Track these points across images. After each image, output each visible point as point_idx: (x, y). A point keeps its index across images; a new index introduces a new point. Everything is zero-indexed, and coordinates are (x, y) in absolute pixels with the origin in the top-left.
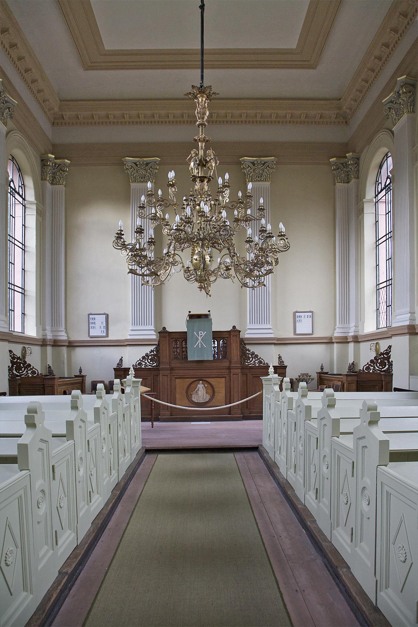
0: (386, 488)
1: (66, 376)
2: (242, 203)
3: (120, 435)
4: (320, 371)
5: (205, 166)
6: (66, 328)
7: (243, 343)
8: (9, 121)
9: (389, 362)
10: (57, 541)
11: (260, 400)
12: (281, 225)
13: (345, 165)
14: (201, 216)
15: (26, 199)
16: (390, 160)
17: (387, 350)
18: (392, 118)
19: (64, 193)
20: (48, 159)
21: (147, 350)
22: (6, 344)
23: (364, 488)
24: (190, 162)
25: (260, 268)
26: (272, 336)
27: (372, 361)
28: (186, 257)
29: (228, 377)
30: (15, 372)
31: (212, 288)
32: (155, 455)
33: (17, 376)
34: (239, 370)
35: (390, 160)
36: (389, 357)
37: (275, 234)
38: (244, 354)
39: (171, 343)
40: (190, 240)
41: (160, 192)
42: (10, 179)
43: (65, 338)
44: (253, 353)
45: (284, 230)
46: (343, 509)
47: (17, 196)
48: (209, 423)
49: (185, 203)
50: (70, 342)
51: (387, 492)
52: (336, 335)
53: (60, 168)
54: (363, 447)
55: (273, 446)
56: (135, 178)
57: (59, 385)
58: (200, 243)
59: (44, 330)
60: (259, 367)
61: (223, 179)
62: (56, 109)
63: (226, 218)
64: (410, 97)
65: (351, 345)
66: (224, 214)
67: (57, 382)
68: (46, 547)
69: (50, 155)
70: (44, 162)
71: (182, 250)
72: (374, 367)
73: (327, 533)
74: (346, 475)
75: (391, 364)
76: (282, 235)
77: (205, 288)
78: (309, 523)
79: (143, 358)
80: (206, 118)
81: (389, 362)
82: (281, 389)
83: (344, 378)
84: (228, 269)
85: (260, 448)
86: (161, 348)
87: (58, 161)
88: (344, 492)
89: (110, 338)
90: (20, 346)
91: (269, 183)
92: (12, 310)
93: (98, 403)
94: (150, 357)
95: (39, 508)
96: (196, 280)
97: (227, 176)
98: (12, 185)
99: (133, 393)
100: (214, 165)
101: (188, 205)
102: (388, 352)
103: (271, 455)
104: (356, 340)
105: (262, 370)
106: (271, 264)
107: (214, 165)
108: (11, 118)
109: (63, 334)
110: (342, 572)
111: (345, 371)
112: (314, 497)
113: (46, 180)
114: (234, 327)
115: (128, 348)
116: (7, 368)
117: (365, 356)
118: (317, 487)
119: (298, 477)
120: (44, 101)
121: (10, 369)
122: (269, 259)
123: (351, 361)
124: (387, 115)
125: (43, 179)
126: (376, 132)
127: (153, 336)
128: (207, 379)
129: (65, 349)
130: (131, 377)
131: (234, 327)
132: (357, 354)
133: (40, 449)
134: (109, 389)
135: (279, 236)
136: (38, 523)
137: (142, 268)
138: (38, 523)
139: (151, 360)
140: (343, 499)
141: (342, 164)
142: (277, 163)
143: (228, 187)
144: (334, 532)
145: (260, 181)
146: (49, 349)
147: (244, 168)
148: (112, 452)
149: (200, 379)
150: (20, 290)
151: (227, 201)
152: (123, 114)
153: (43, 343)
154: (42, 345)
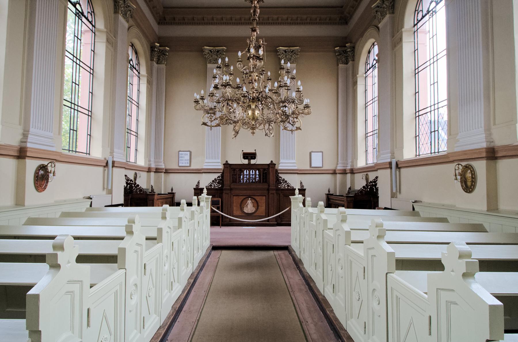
0: (395, 293)
1: (163, 193)
3: (195, 236)
4: (327, 193)
6: (164, 161)
8: (130, 19)
9: (376, 188)
10: (144, 325)
11: (289, 212)
13: (345, 52)
15: (96, 26)
16: (376, 48)
20: (155, 47)
21: (216, 176)
22: (123, 170)
23: (374, 290)
26: (296, 168)
34: (275, 191)
35: (376, 48)
36: (376, 185)
38: (278, 180)
39: (231, 171)
42: (130, 58)
43: (163, 167)
44: (284, 180)
46: (356, 305)
47: (134, 70)
50: (166, 170)
51: (397, 297)
52: (339, 168)
54: (372, 256)
55: (298, 246)
57: (158, 199)
59: (150, 161)
60: (288, 189)
62: (161, 13)
65: (349, 176)
67: (156, 197)
68: (135, 331)
69: (156, 44)
70: (152, 48)
73: (322, 291)
74: (358, 276)
78: (328, 312)
79: (213, 181)
81: (376, 188)
82: (304, 205)
86: (225, 174)
87: (161, 48)
88: (356, 290)
90: (133, 172)
91: (295, 65)
98: (131, 63)
103: (297, 253)
104: (352, 172)
105: (290, 192)
108: (132, 17)
109: (162, 164)
110: (342, 333)
112: (363, 333)
113: (153, 60)
114: (272, 161)
115: (204, 174)
117: (360, 183)
118: (333, 283)
119: (318, 273)
120: (153, 8)
123: (348, 186)
124: (375, 16)
125: (152, 60)
126: (366, 30)
127: (221, 167)
128: (253, 197)
129: (163, 174)
130: (204, 195)
132: (353, 182)
133: (136, 251)
136: (130, 311)
139: (218, 183)
140: (355, 296)
144: (349, 322)
146: (152, 174)
148: (189, 250)
150: (135, 134)
152: (203, 18)
153: (149, 170)
154: (147, 172)
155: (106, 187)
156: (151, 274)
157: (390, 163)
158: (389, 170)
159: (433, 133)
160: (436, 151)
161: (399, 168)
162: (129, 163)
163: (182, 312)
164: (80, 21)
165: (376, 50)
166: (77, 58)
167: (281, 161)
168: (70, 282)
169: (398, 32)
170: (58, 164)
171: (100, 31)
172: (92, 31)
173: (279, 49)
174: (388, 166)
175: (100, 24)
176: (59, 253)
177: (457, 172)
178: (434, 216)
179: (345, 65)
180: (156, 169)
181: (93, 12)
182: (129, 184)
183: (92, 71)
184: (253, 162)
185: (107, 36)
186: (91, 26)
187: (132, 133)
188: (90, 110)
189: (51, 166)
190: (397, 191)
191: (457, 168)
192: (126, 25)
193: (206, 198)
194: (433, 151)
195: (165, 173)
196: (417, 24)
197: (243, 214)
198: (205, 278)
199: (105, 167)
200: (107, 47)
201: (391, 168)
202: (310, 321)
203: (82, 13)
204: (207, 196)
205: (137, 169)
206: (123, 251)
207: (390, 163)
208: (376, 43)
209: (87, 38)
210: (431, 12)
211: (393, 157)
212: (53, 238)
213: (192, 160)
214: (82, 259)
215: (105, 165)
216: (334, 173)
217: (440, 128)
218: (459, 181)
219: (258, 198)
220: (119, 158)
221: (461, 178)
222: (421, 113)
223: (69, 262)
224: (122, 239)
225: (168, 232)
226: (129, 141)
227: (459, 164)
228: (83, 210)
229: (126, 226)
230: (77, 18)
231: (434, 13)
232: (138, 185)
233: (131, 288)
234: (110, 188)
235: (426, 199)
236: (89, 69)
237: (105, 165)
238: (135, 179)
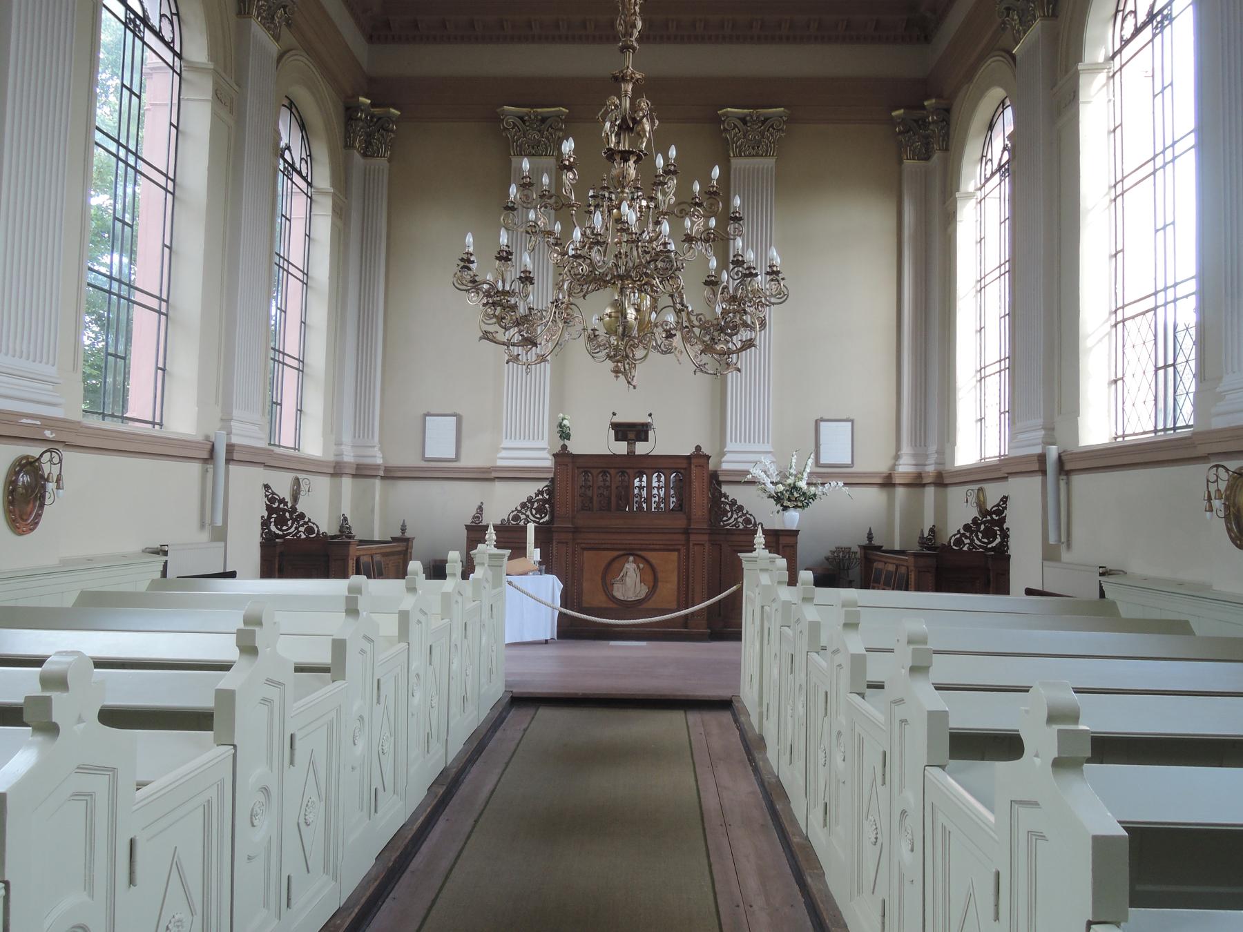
0: (941, 819)
1: (376, 538)
2: (700, 205)
3: (454, 666)
4: (866, 542)
5: (631, 130)
6: (381, 442)
7: (715, 480)
8: (285, 31)
9: (1002, 529)
10: (289, 899)
11: (736, 599)
12: (774, 253)
13: (922, 123)
14: (622, 230)
15: (184, 55)
16: (1009, 113)
17: (998, 505)
18: (1013, 28)
19: (386, 172)
24: (604, 122)
25: (731, 336)
27: (966, 527)
28: (596, 310)
29: (683, 551)
30: (273, 528)
31: (640, 372)
32: (531, 711)
33: (278, 536)
35: (1009, 113)
36: (1003, 520)
37: (761, 270)
40: (597, 280)
41: (545, 180)
42: (283, 144)
43: (379, 461)
44: (734, 502)
45: (777, 261)
46: (870, 853)
47: (296, 178)
48: (644, 644)
49: (591, 201)
50: (387, 469)
51: (944, 828)
53: (380, 124)
54: (902, 721)
55: (757, 699)
56: (521, 146)
58: (619, 284)
59: (339, 443)
61: (666, 158)
63: (669, 236)
64: (943, 128)
65: (930, 492)
66: (666, 227)
69: (362, 99)
70: (350, 112)
71: (584, 296)
72: (972, 540)
75: (1005, 536)
76: (773, 273)
77: (625, 373)
79: (523, 505)
80: (636, 34)
81: (1002, 529)
83: (911, 560)
84: (670, 336)
85: (735, 704)
87: (376, 111)
89: (465, 462)
90: (288, 477)
91: (774, 160)
92: (277, 404)
93: (408, 602)
94: (536, 505)
95: (253, 826)
96: (609, 357)
97: (673, 152)
98: (287, 155)
99: (490, 579)
100: (647, 128)
101: (597, 206)
102: (1000, 509)
103: (754, 720)
104: (942, 481)
106: (753, 329)
107: (647, 128)
108: (288, 25)
111: (915, 547)
113: (353, 147)
114: (698, 448)
116: (259, 521)
117: (960, 512)
121: (265, 523)
122: (748, 319)
124: (1004, 23)
125: (348, 145)
126: (981, 59)
127: (549, 463)
129: (377, 482)
131: (698, 448)
132: (941, 509)
133: (265, 701)
134: (437, 571)
135: (768, 273)
136: (250, 858)
137: (506, 329)
138: (250, 858)
139: (539, 510)
141: (916, 121)
142: (791, 120)
143: (675, 173)
145: (757, 155)
146: (347, 482)
147: (725, 129)
149: (629, 551)
150: (295, 363)
151: (672, 201)
153: (336, 471)
154: (332, 475)
155: (208, 520)
156: (312, 763)
157: (1042, 458)
158: (1038, 479)
159: (1161, 373)
160: (1170, 425)
161: (1068, 473)
162: (276, 450)
163: (406, 877)
164: (138, 43)
165: (1007, 122)
166: (128, 150)
167: (730, 446)
168: (82, 769)
169: (1067, 72)
170: (69, 456)
171: (194, 67)
172: (172, 68)
173: (724, 115)
174: (1036, 467)
175: (197, 51)
176: (55, 695)
177: (1213, 488)
178: (1155, 615)
179: (922, 163)
180: (359, 467)
181: (177, 14)
182: (277, 510)
183: (170, 184)
184: (641, 448)
185: (215, 83)
186: (168, 56)
187: (287, 360)
188: (164, 297)
189: (51, 461)
190: (1060, 540)
191: (1213, 478)
192: (274, 48)
193: (492, 556)
194: (1160, 427)
195: (382, 478)
196: (1120, 51)
197: (612, 605)
198: (482, 780)
199: (205, 461)
200: (214, 114)
201: (1043, 472)
202: (758, 902)
203: (145, 20)
204: (496, 551)
205: (300, 466)
206: (226, 698)
207: (1042, 458)
208: (1008, 102)
209: (159, 88)
210: (1159, 18)
211: (1049, 441)
212: (37, 662)
213: (465, 444)
214: (114, 717)
215: (206, 456)
216: (887, 483)
217: (1181, 359)
218: (1222, 514)
219: (653, 556)
220: (248, 434)
221: (1227, 507)
222: (1129, 311)
223: (80, 720)
224: (225, 667)
225: (363, 651)
226: (273, 384)
227: (1217, 466)
228: (143, 587)
229: (240, 633)
230: (130, 35)
231: (1166, 23)
232: (302, 516)
233: (248, 798)
234: (219, 523)
235: (1138, 566)
236: (162, 180)
237: (206, 456)
238: (295, 498)
